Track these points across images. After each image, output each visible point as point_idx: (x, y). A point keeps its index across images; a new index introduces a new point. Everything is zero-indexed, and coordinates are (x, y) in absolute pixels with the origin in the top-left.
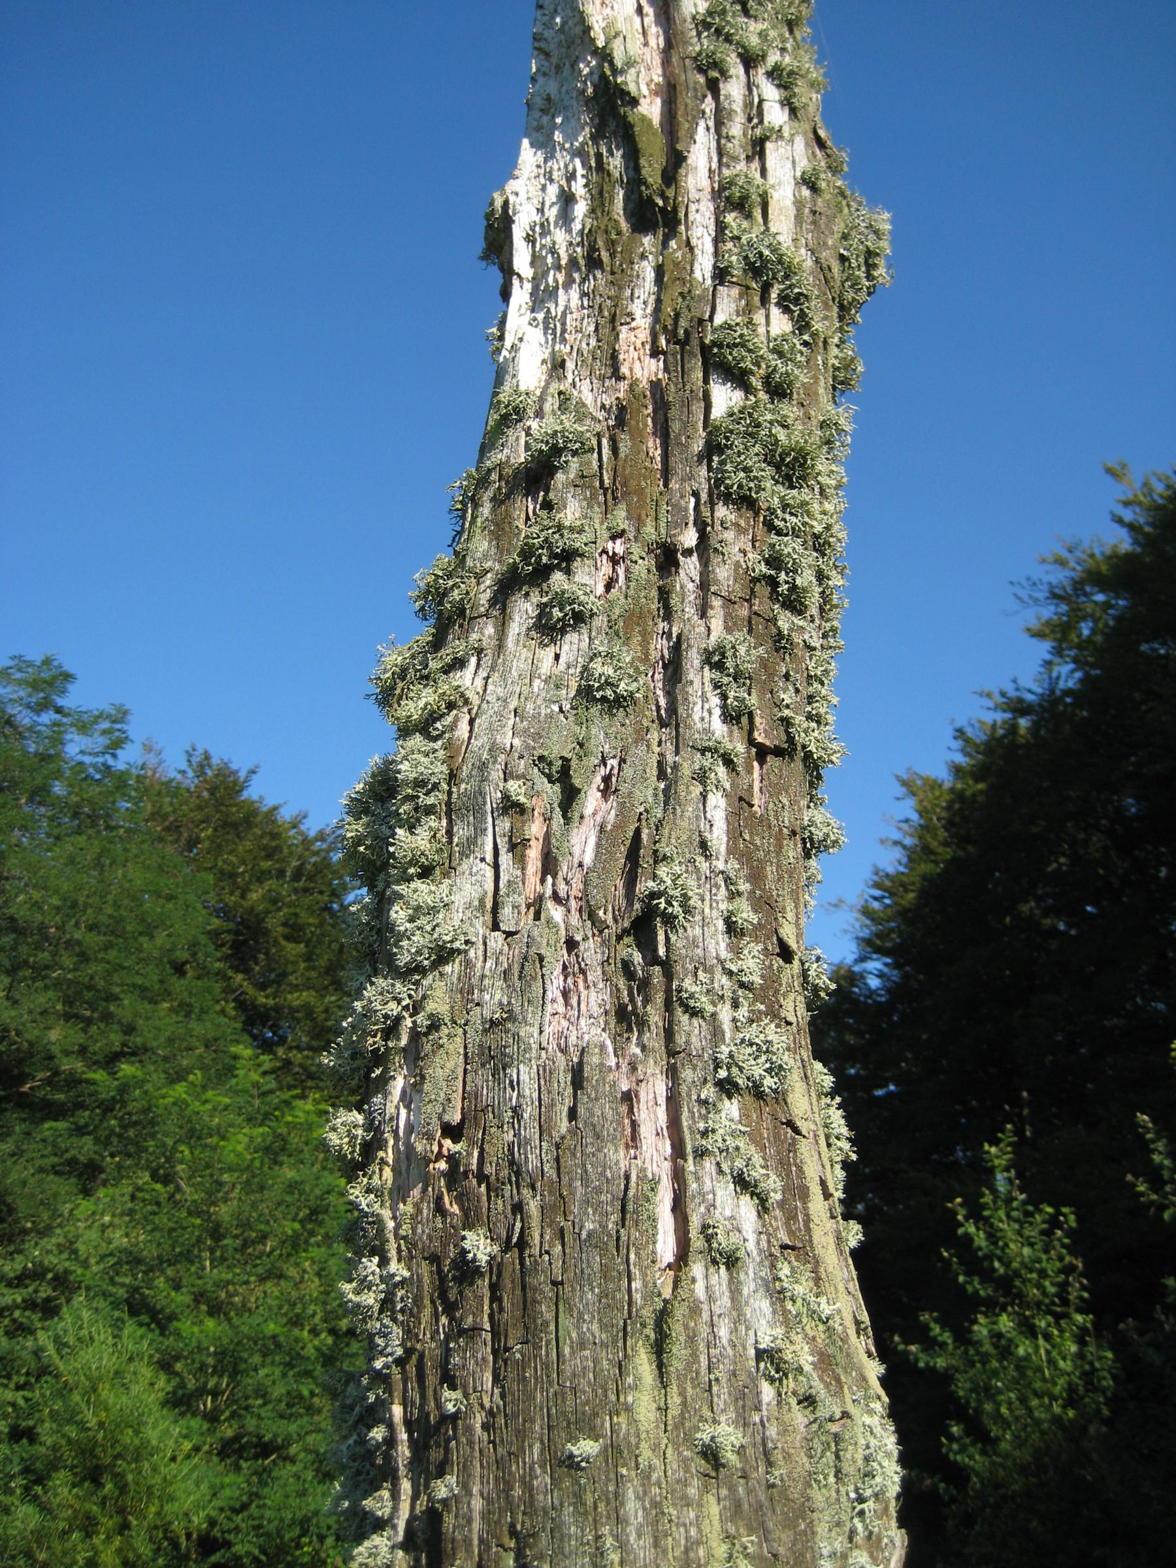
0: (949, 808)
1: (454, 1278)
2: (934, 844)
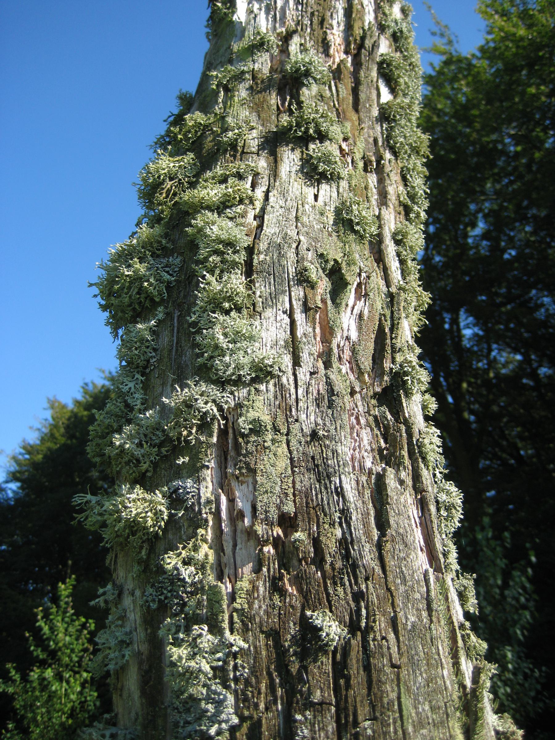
0: (69, 419)
1: (295, 653)
2: (57, 435)
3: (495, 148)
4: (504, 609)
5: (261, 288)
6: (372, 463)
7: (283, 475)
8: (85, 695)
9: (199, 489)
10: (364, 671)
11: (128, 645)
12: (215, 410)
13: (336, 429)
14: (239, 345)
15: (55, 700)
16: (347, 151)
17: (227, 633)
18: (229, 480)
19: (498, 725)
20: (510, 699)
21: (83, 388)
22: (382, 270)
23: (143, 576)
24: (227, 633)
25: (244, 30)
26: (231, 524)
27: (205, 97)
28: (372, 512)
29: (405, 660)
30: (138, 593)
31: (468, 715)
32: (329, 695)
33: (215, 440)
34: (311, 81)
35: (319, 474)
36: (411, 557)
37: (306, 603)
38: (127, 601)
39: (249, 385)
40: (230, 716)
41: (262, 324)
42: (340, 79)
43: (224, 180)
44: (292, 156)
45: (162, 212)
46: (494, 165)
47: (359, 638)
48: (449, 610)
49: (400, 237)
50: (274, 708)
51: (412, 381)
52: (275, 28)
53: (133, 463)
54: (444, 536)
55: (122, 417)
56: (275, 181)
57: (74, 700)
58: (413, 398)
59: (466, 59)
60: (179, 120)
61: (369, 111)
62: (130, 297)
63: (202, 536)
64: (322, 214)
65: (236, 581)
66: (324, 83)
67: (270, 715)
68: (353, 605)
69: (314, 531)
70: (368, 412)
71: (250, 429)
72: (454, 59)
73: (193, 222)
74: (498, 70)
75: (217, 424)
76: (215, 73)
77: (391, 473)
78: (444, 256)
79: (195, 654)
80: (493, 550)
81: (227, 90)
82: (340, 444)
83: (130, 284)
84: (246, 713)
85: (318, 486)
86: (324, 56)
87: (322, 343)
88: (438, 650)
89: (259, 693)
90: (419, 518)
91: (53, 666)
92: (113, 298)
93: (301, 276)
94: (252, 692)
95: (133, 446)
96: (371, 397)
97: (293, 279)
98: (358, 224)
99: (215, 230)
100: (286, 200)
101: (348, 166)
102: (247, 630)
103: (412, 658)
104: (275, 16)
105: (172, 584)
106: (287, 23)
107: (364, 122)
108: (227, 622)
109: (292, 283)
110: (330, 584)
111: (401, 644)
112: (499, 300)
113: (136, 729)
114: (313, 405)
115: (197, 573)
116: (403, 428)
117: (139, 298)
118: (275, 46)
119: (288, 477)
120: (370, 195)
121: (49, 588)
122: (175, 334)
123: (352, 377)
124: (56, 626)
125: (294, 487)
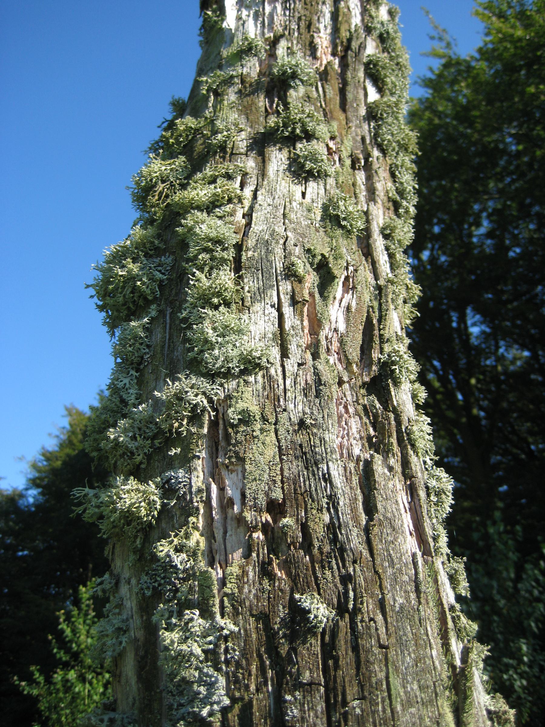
2: (75, 441)
3: (496, 148)
4: (518, 602)
5: (250, 283)
6: (361, 450)
7: (271, 463)
8: (108, 695)
9: (190, 479)
10: (353, 652)
11: (125, 632)
12: (205, 402)
13: (323, 417)
14: (227, 338)
15: (78, 701)
16: (334, 149)
17: (218, 617)
18: (220, 470)
19: (490, 705)
20: (526, 691)
21: (99, 394)
22: (370, 264)
23: (138, 565)
24: (218, 617)
25: (232, 37)
26: (222, 512)
27: (197, 102)
28: (360, 498)
29: (393, 640)
30: (134, 581)
31: (457, 694)
32: (318, 675)
33: (205, 431)
34: (298, 82)
35: (307, 462)
36: (399, 540)
37: (296, 585)
38: (124, 590)
39: (238, 377)
40: (221, 698)
41: (250, 318)
42: (326, 81)
43: (213, 181)
44: (280, 156)
45: (155, 213)
46: (496, 165)
47: (347, 619)
48: (439, 592)
49: (388, 232)
50: (265, 689)
51: (400, 371)
52: (263, 34)
53: (128, 456)
54: (434, 521)
55: (118, 412)
56: (263, 180)
57: (97, 700)
58: (403, 387)
59: (465, 61)
60: (171, 126)
61: (357, 110)
62: (124, 296)
63: (193, 523)
64: (309, 211)
65: (227, 566)
66: (311, 85)
67: (261, 696)
68: (341, 588)
69: (302, 517)
70: (357, 401)
71: (239, 419)
72: (453, 62)
73: (183, 221)
74: (497, 71)
75: (207, 416)
76: (205, 79)
77: (378, 459)
78: (451, 255)
79: (187, 638)
80: (505, 544)
81: (217, 94)
82: (327, 432)
83: (124, 284)
84: (237, 694)
85: (305, 473)
86: (311, 58)
87: (311, 335)
88: (427, 630)
89: (250, 675)
90: (409, 503)
91: (76, 668)
92: (108, 298)
93: (289, 271)
94: (243, 674)
95: (127, 439)
96: (360, 387)
97: (281, 274)
98: (345, 219)
99: (204, 228)
100: (274, 198)
101: (335, 163)
102: (238, 614)
103: (401, 638)
104: (263, 23)
105: (165, 571)
106: (275, 28)
107: (352, 121)
108: (217, 606)
109: (279, 278)
110: (319, 567)
111: (389, 625)
112: (505, 297)
113: (133, 714)
114: (301, 395)
115: (189, 560)
116: (392, 416)
117: (133, 297)
118: (263, 51)
119: (276, 465)
120: (358, 191)
121: (71, 591)
122: (167, 331)
123: (340, 367)
124: (78, 628)
125: (282, 474)
